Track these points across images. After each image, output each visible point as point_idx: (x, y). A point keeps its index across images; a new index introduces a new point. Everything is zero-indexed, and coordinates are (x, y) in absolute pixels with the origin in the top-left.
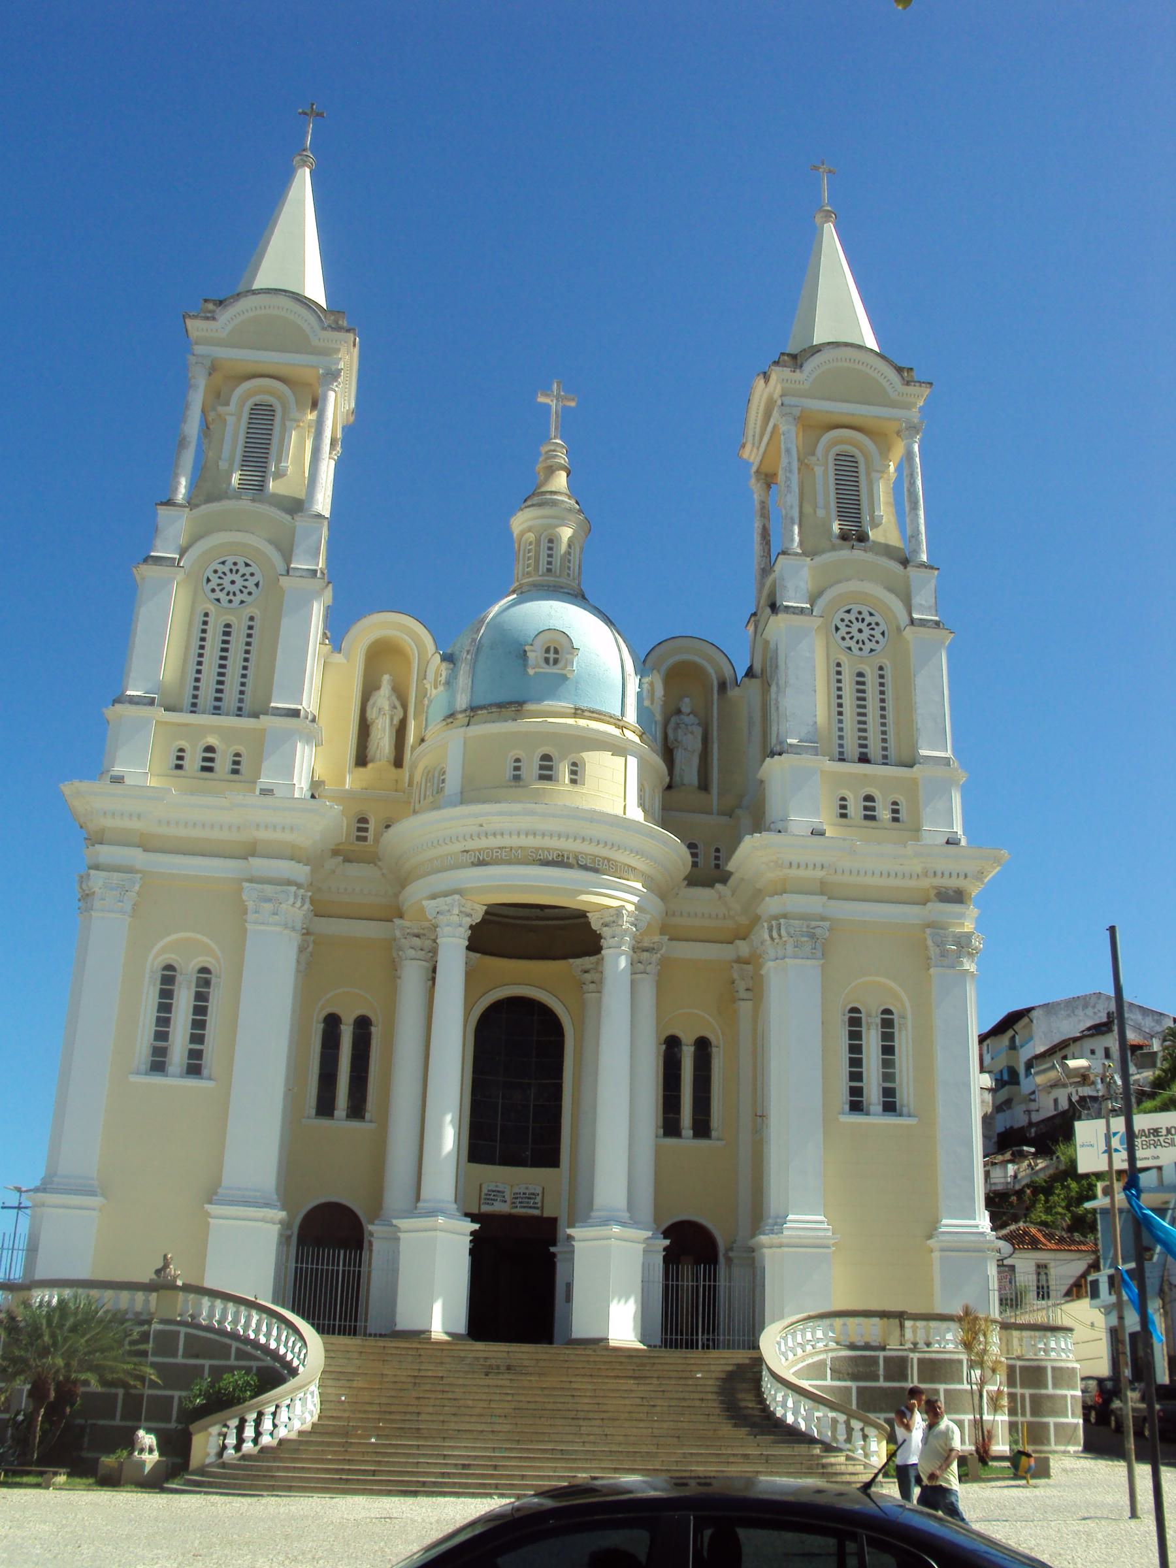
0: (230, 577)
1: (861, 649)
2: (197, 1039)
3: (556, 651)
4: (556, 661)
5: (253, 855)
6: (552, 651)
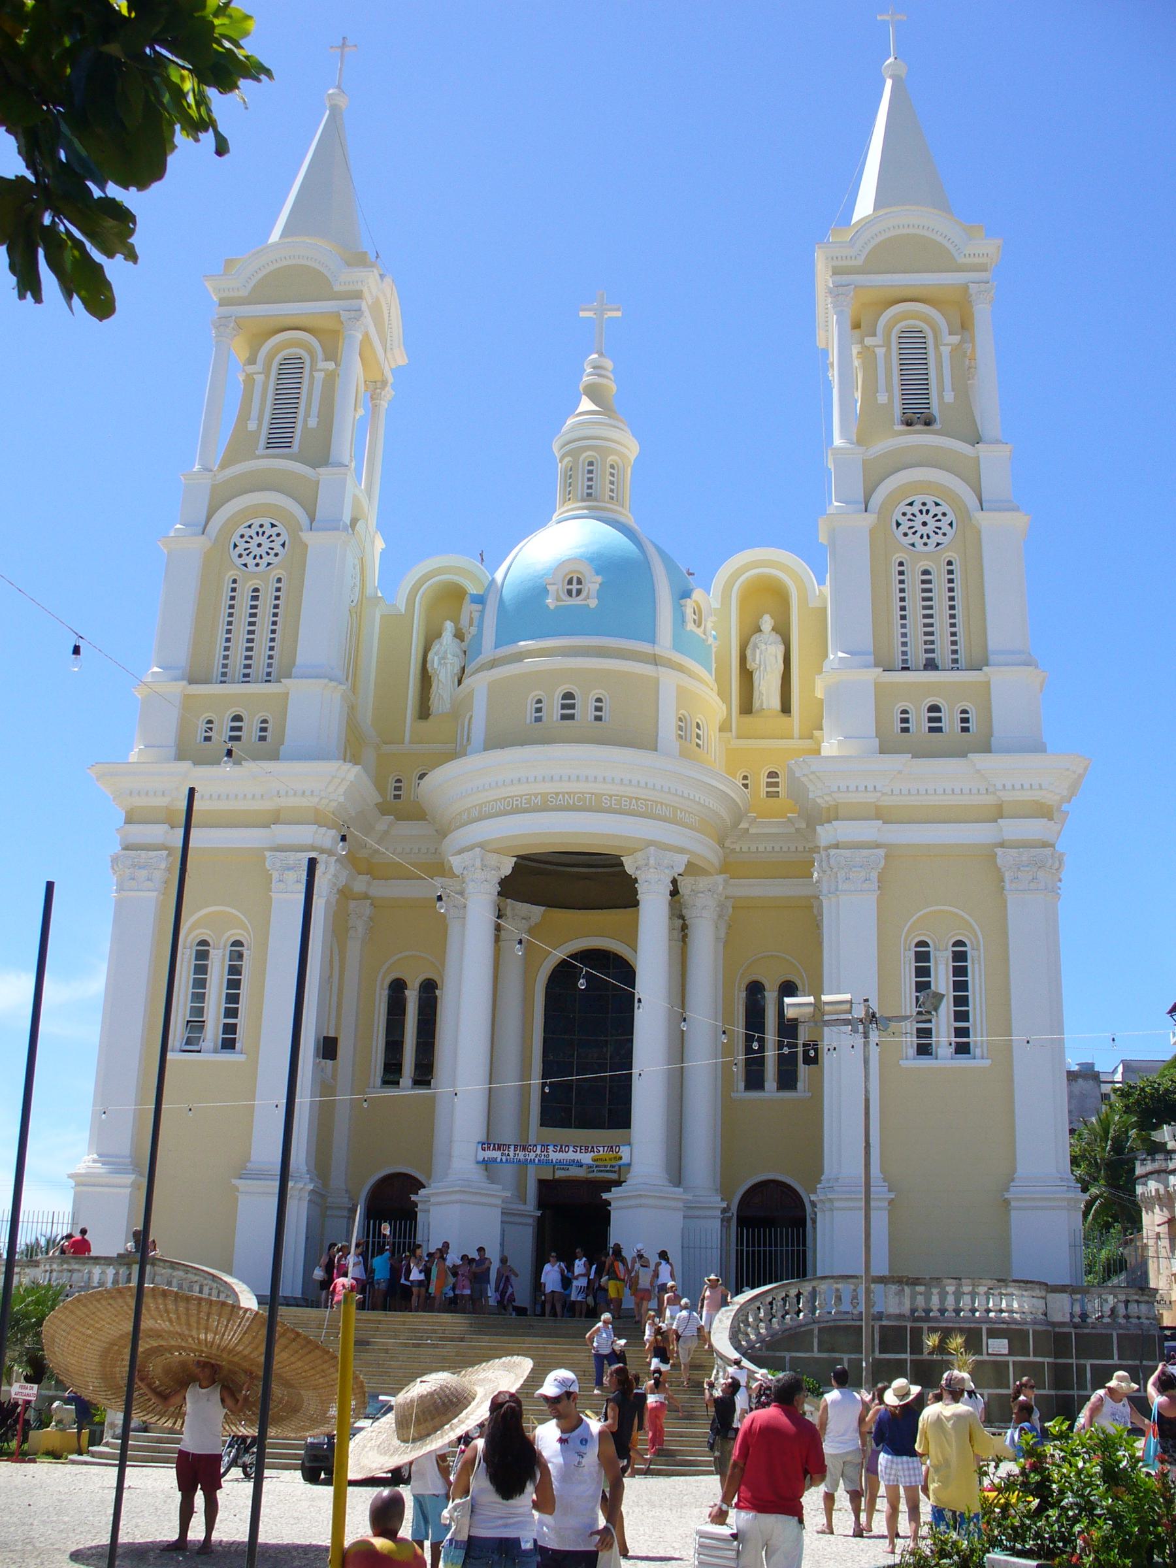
0: (257, 540)
1: (276, 555)
2: (232, 1013)
3: (579, 582)
4: (579, 592)
5: (837, 819)
6: (575, 582)
